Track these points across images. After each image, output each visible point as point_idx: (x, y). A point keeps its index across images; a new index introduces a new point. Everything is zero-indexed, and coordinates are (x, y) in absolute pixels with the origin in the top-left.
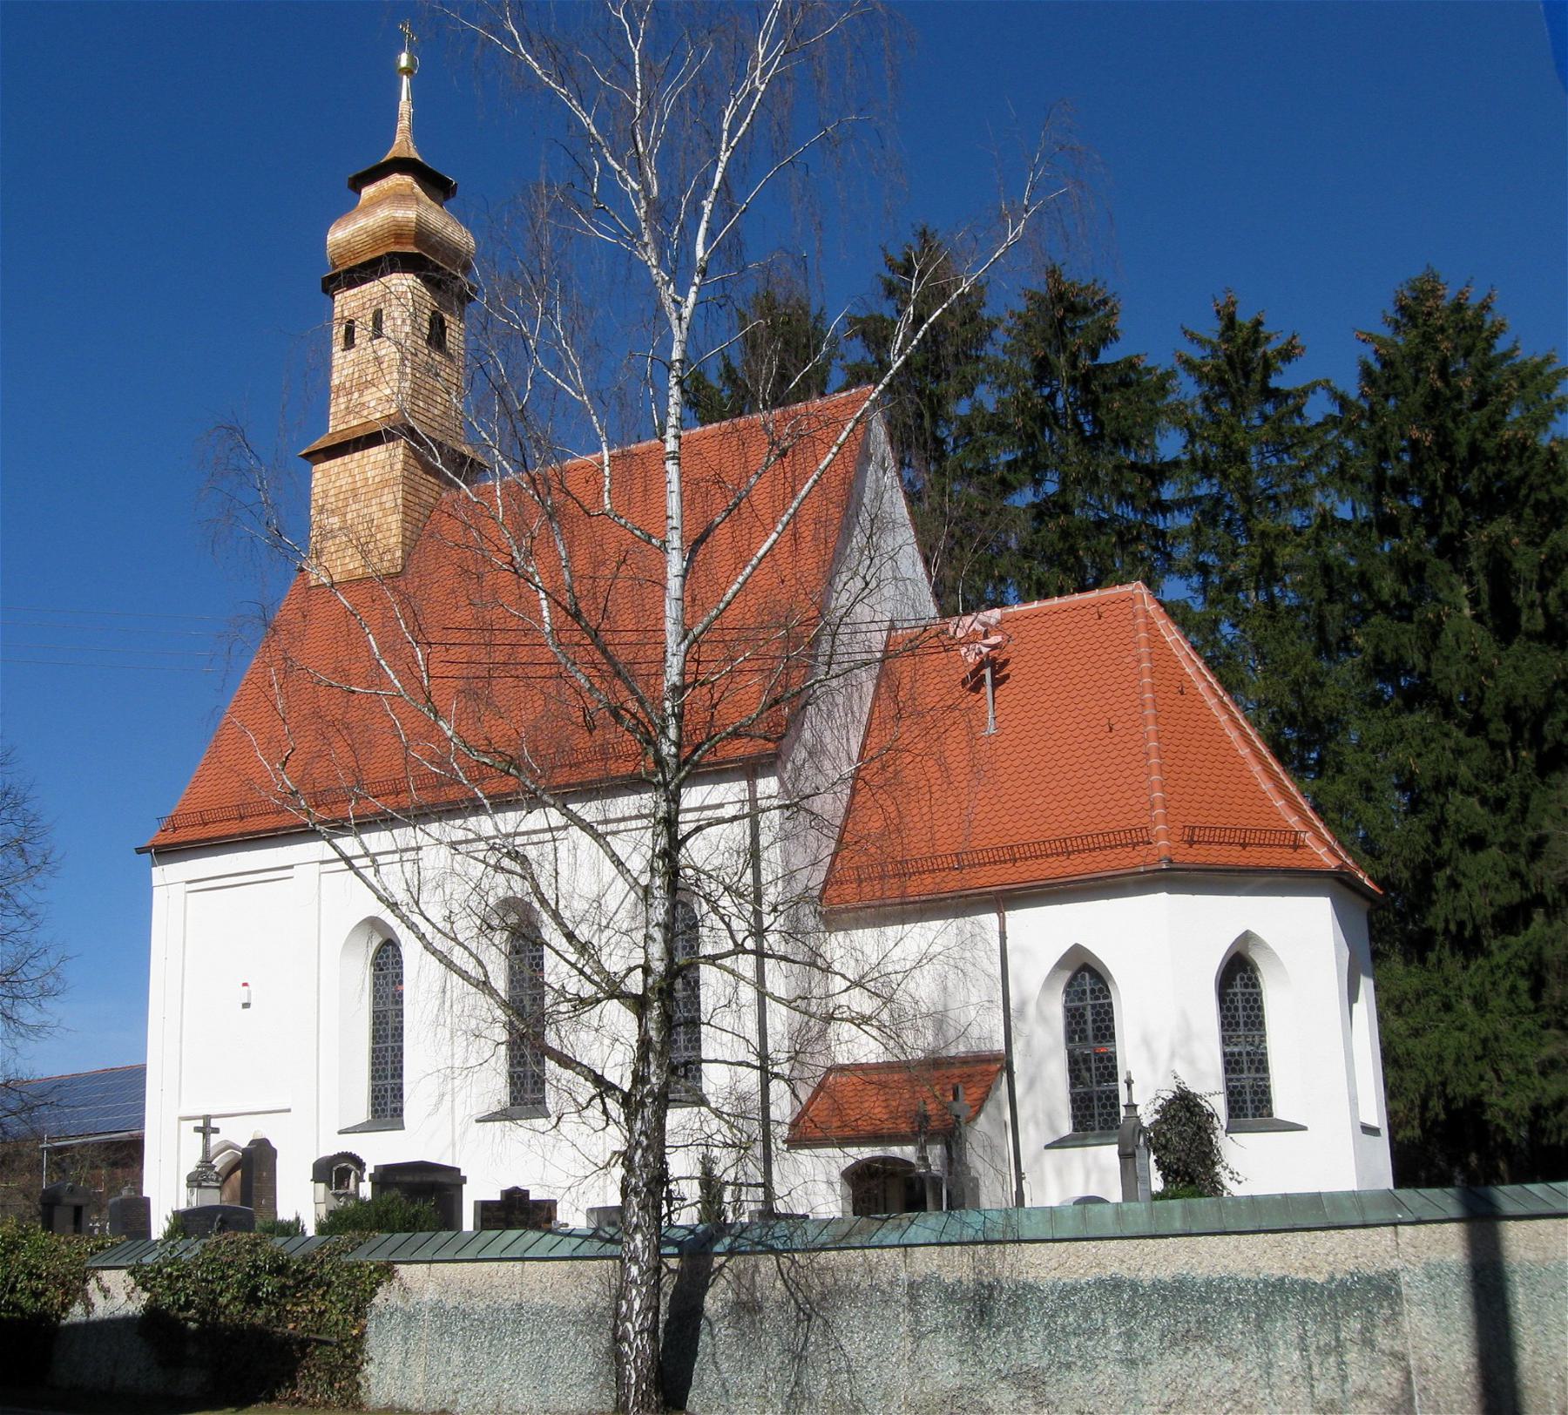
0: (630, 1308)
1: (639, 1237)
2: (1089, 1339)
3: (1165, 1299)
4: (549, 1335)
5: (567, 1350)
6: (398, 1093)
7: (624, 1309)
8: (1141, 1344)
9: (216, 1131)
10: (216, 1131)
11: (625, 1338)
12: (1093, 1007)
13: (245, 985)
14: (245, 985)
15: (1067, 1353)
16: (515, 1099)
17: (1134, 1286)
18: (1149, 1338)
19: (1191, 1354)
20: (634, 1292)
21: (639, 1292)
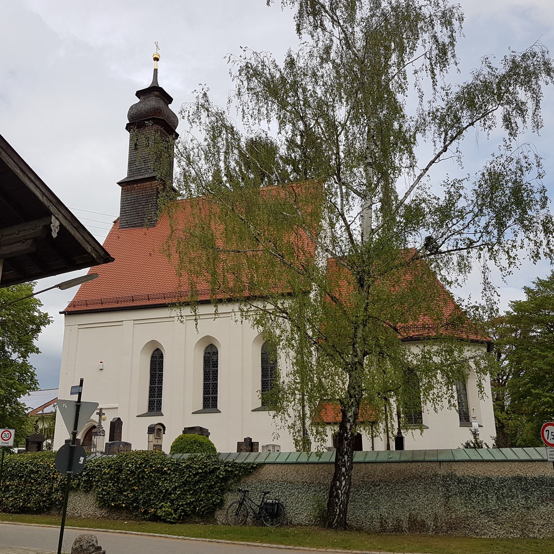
0: (341, 484)
1: (346, 457)
2: (512, 499)
3: (537, 485)
4: (286, 493)
5: (294, 499)
6: (160, 403)
7: (338, 484)
8: (531, 501)
9: (104, 414)
10: (104, 414)
11: (337, 496)
12: (212, 384)
13: (101, 362)
14: (101, 362)
15: (504, 504)
16: (263, 404)
17: (526, 479)
18: (533, 499)
19: (549, 506)
20: (343, 478)
21: (345, 478)
